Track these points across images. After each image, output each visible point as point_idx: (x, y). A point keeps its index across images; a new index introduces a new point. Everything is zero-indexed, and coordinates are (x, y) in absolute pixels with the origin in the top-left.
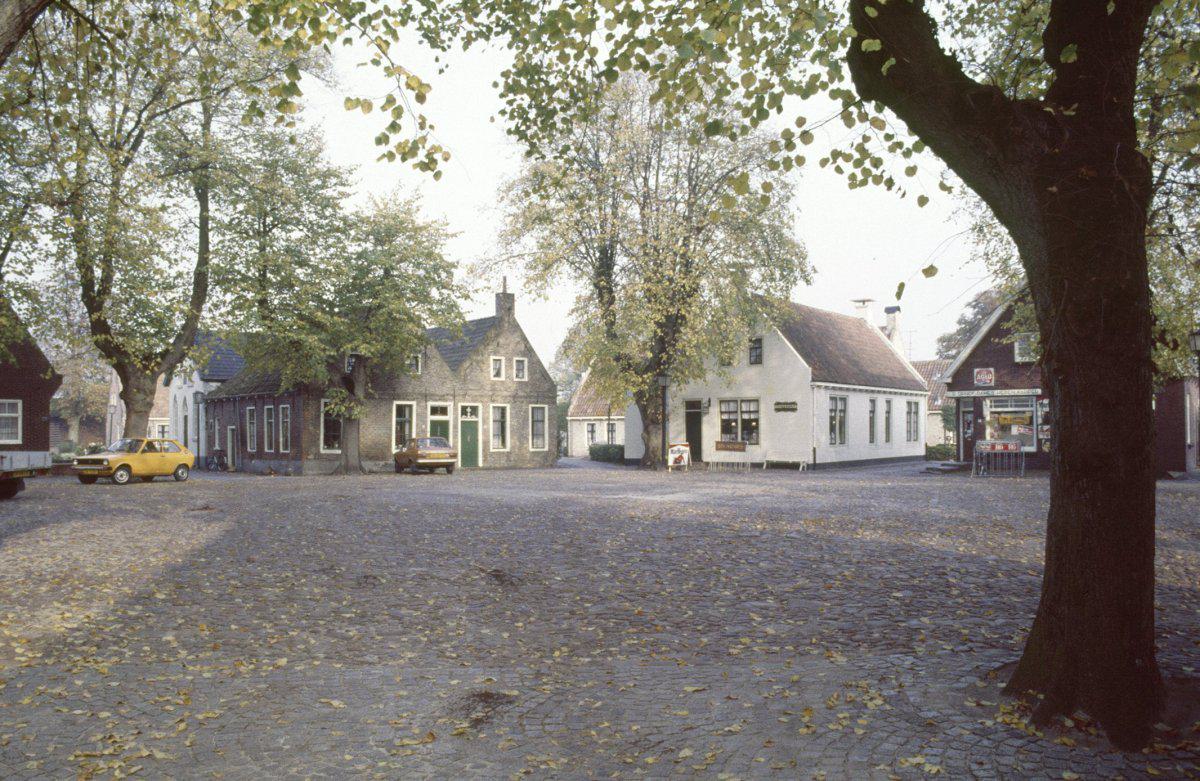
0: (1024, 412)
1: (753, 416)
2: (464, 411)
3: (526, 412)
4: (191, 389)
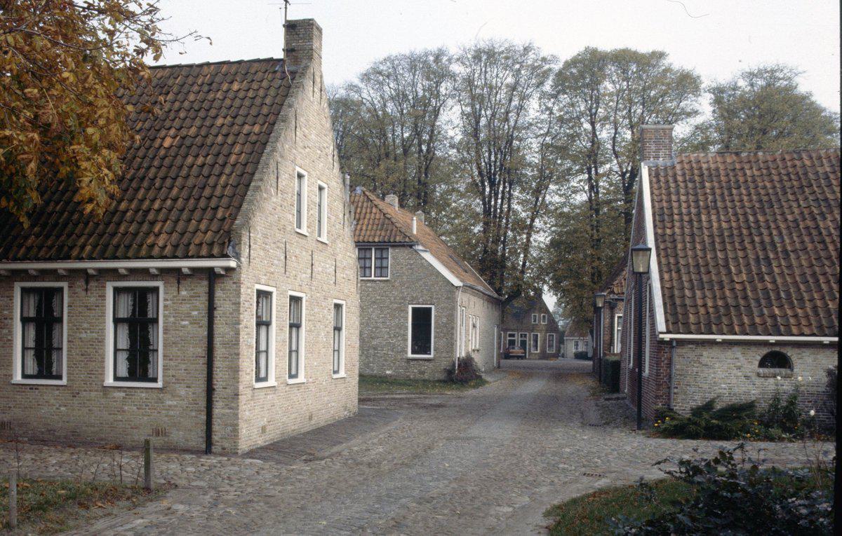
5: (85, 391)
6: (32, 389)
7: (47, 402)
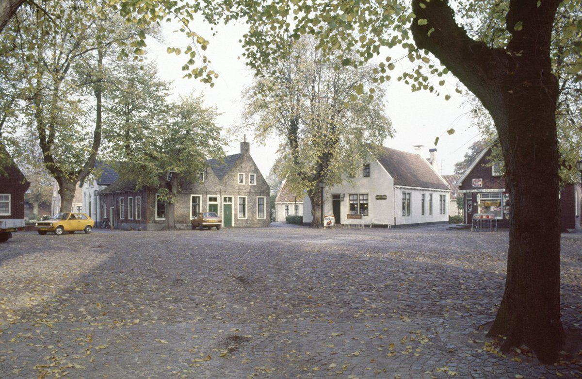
0: (497, 200)
1: (365, 202)
2: (225, 199)
3: (255, 200)
4: (93, 189)
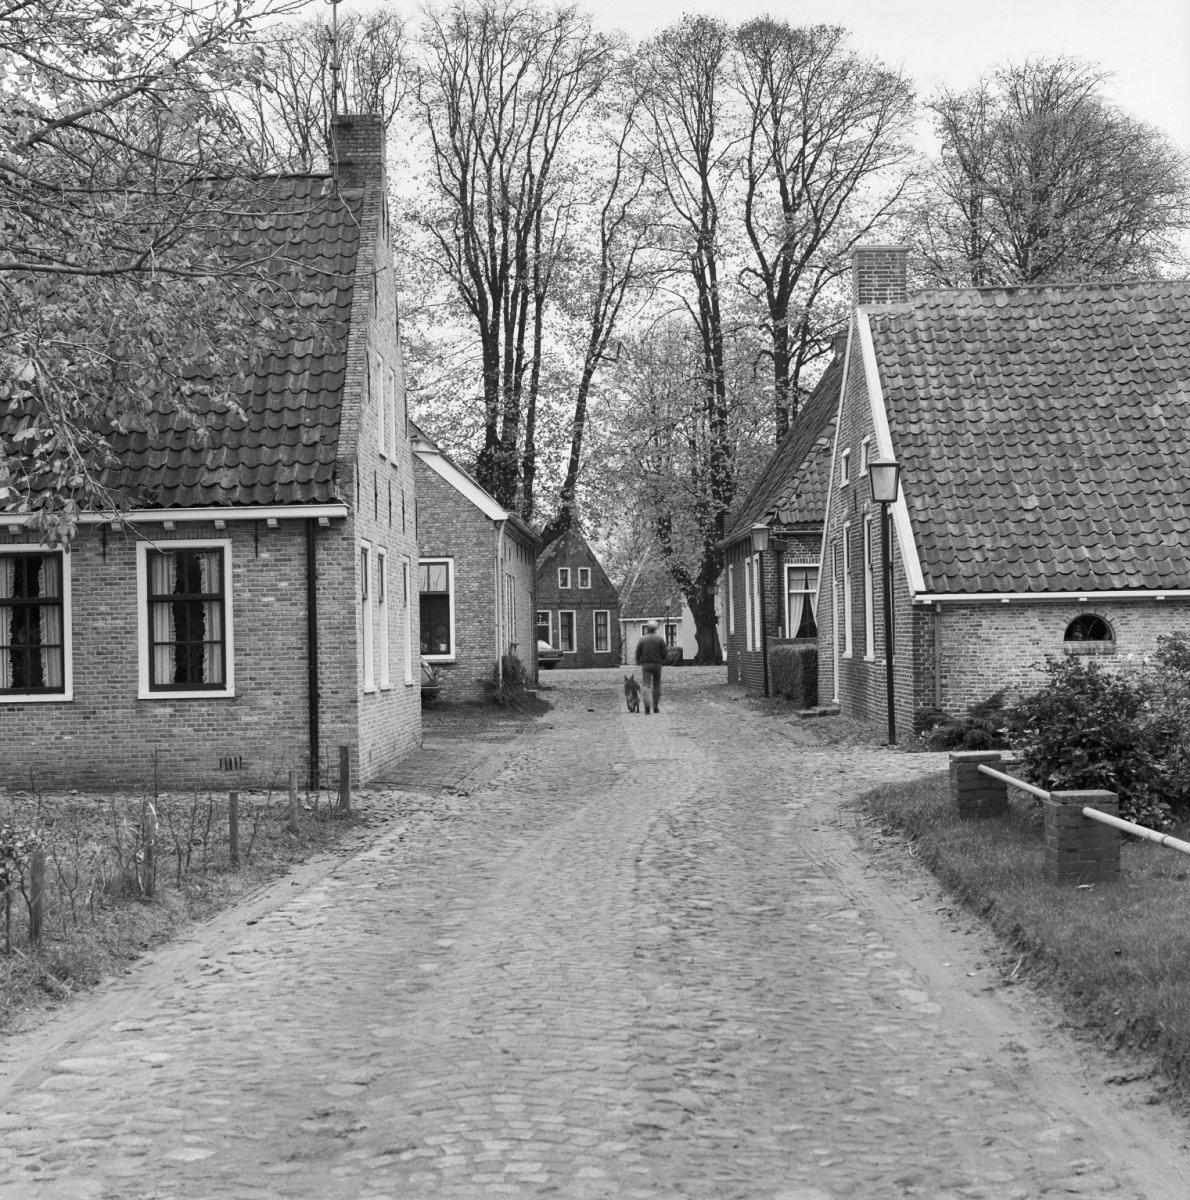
3: (591, 617)
5: (106, 708)
6: (13, 710)
7: (38, 729)
